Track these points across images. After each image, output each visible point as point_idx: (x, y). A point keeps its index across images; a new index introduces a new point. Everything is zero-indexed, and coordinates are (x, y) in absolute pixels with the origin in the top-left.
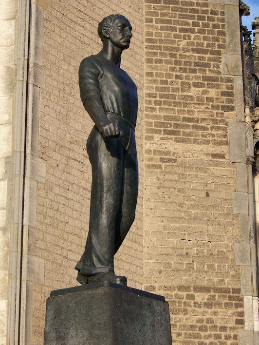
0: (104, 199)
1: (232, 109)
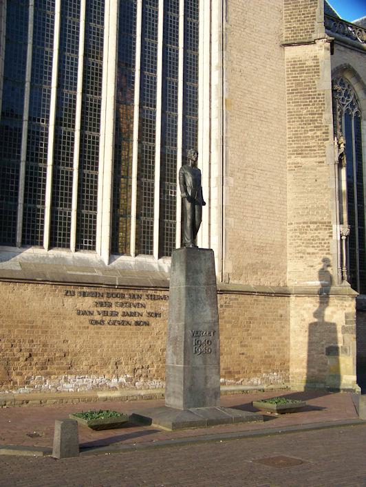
1: (328, 140)
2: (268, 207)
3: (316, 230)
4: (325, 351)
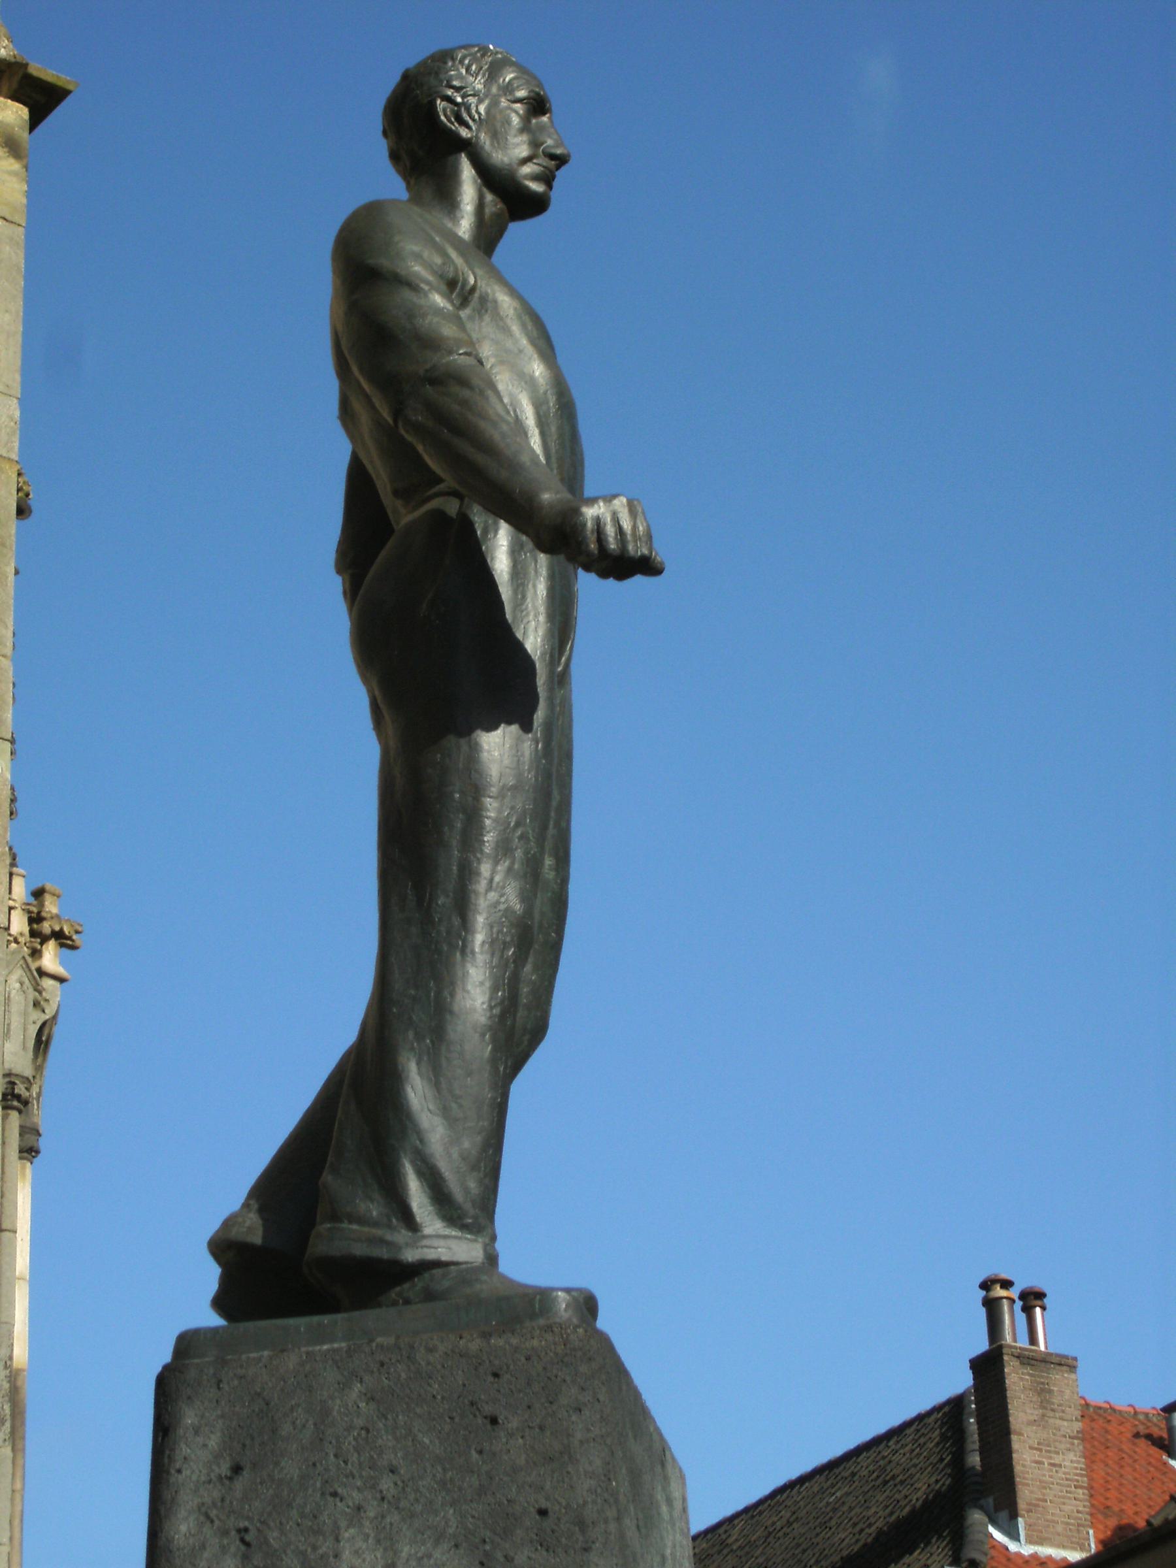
0: (482, 885)
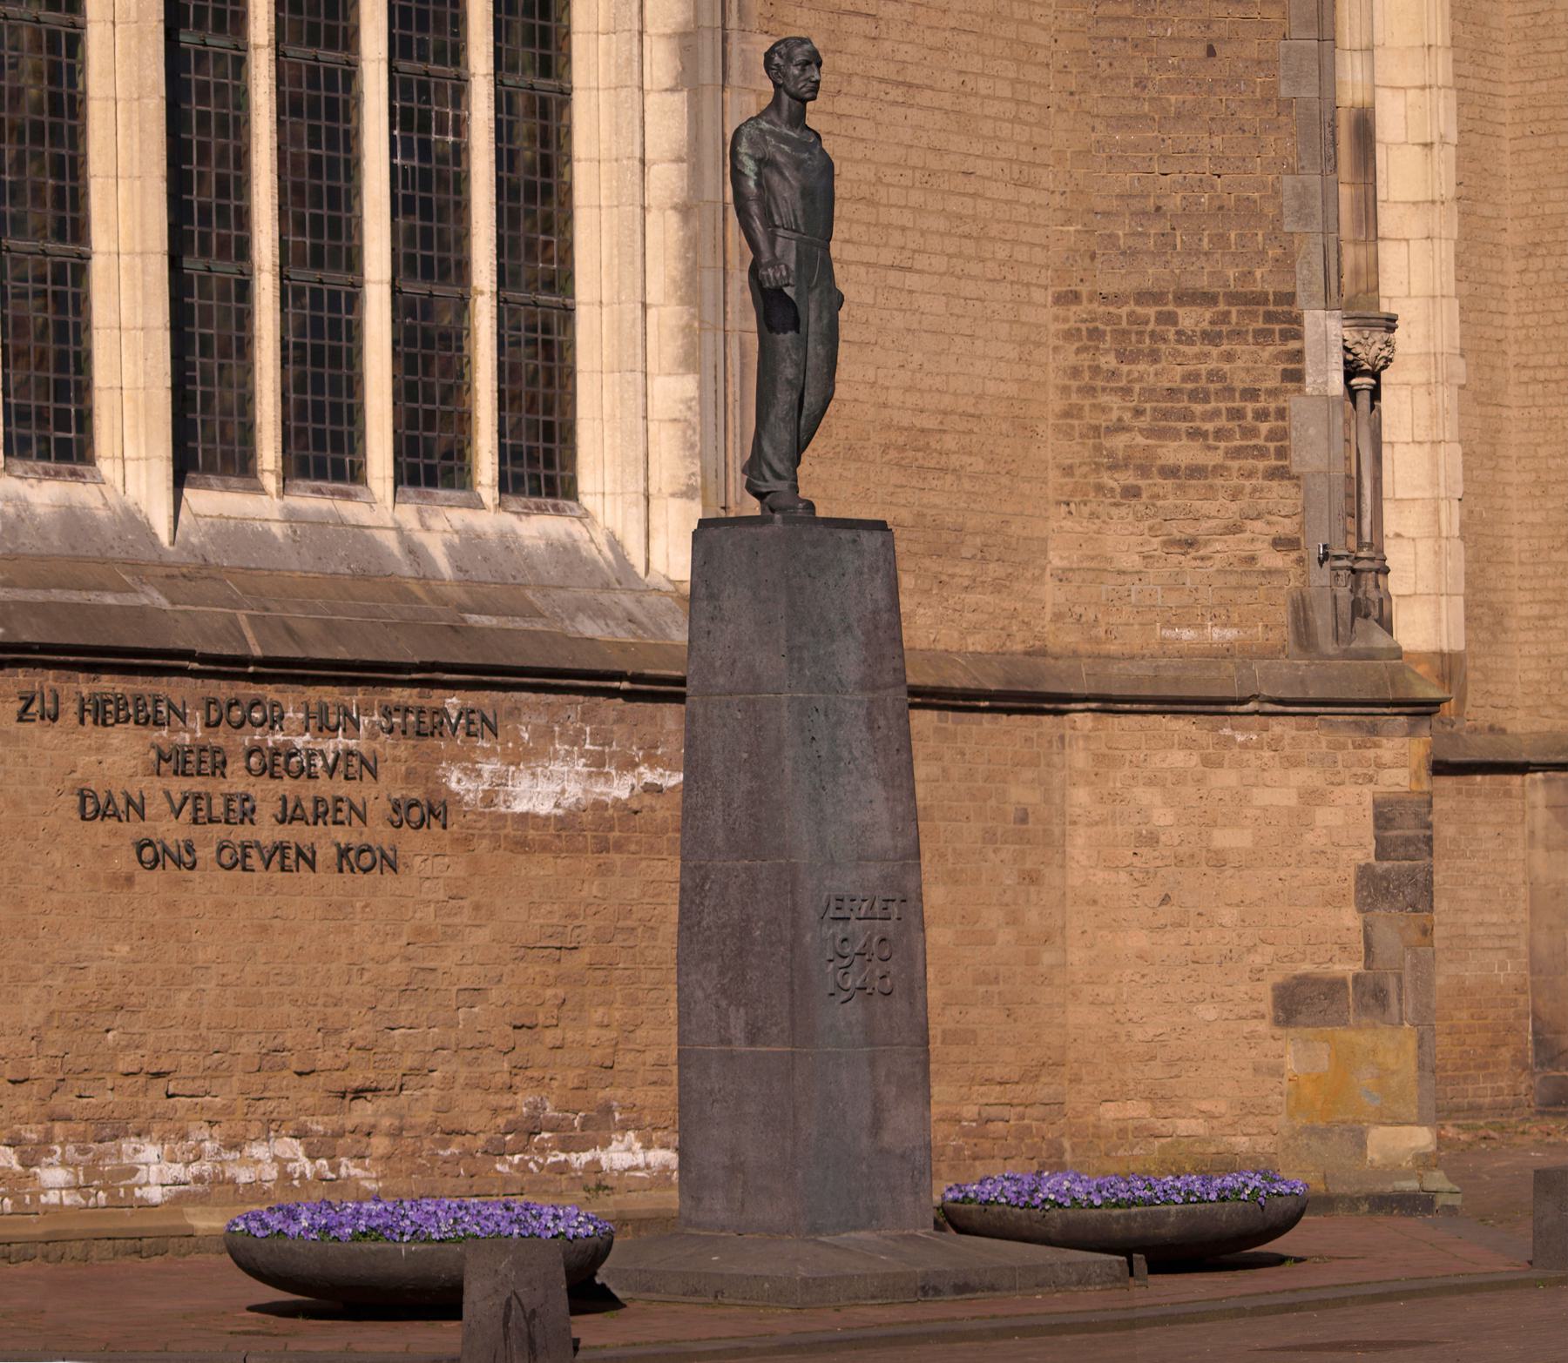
2: (953, 205)
3: (1207, 337)
4: (1266, 1006)
